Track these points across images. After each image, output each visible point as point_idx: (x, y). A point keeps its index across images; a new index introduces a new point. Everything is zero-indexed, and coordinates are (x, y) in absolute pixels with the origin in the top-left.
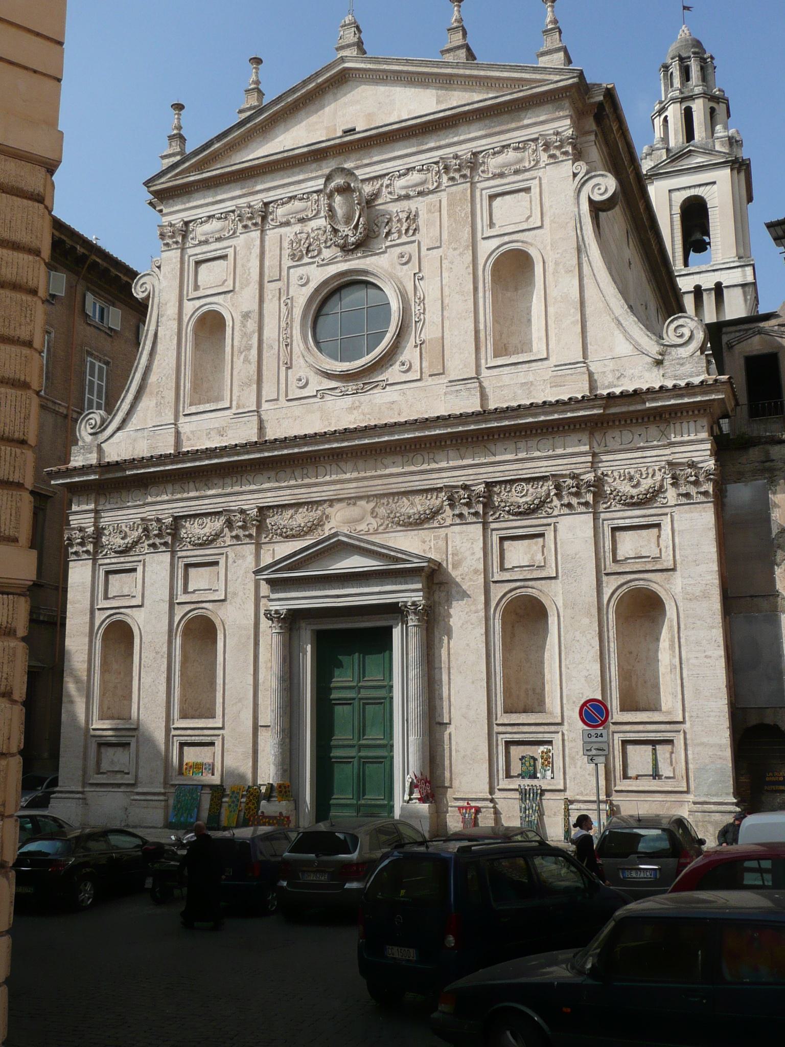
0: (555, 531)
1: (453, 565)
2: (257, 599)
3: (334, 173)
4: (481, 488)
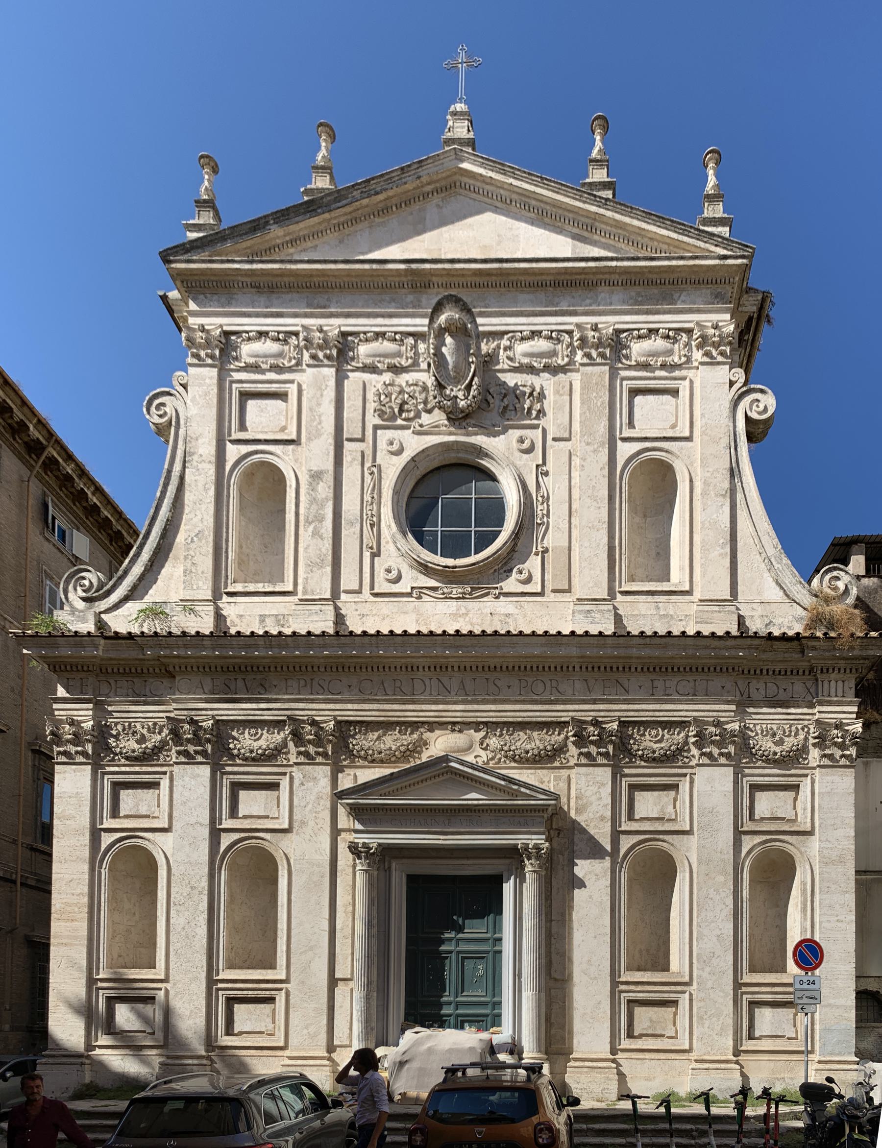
0: (692, 782)
1: (577, 809)
2: (336, 832)
3: (445, 302)
4: (615, 726)
